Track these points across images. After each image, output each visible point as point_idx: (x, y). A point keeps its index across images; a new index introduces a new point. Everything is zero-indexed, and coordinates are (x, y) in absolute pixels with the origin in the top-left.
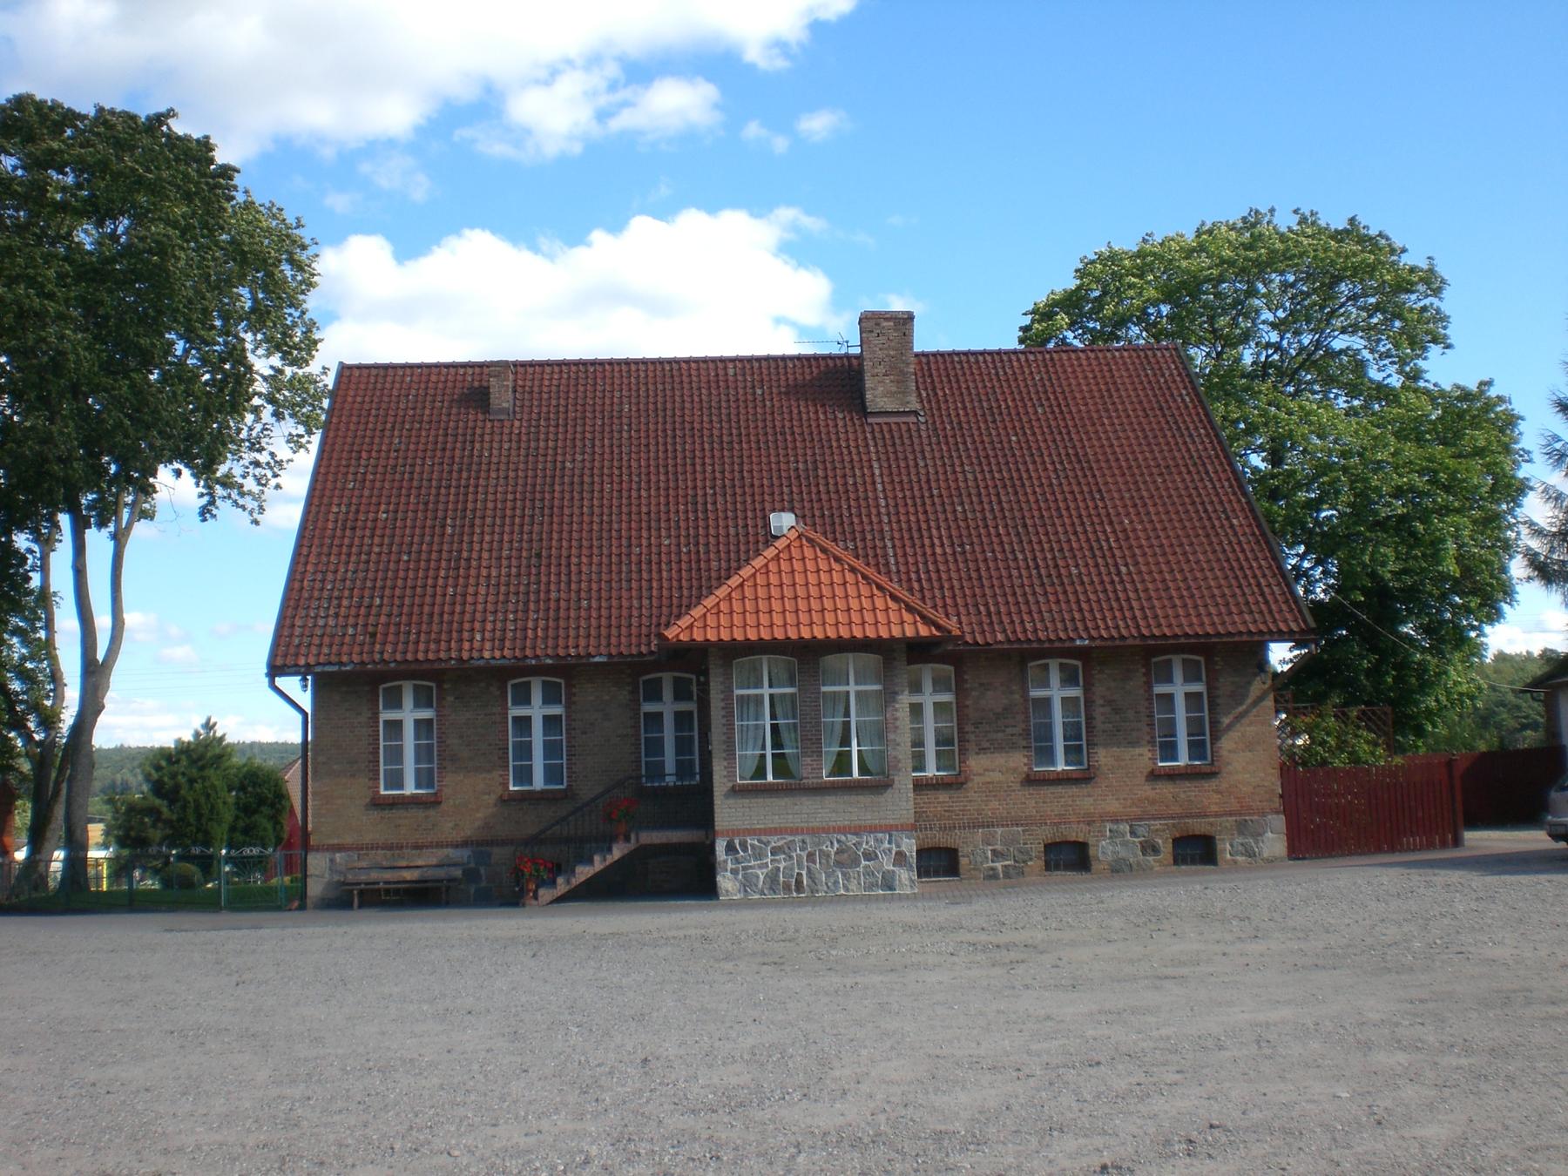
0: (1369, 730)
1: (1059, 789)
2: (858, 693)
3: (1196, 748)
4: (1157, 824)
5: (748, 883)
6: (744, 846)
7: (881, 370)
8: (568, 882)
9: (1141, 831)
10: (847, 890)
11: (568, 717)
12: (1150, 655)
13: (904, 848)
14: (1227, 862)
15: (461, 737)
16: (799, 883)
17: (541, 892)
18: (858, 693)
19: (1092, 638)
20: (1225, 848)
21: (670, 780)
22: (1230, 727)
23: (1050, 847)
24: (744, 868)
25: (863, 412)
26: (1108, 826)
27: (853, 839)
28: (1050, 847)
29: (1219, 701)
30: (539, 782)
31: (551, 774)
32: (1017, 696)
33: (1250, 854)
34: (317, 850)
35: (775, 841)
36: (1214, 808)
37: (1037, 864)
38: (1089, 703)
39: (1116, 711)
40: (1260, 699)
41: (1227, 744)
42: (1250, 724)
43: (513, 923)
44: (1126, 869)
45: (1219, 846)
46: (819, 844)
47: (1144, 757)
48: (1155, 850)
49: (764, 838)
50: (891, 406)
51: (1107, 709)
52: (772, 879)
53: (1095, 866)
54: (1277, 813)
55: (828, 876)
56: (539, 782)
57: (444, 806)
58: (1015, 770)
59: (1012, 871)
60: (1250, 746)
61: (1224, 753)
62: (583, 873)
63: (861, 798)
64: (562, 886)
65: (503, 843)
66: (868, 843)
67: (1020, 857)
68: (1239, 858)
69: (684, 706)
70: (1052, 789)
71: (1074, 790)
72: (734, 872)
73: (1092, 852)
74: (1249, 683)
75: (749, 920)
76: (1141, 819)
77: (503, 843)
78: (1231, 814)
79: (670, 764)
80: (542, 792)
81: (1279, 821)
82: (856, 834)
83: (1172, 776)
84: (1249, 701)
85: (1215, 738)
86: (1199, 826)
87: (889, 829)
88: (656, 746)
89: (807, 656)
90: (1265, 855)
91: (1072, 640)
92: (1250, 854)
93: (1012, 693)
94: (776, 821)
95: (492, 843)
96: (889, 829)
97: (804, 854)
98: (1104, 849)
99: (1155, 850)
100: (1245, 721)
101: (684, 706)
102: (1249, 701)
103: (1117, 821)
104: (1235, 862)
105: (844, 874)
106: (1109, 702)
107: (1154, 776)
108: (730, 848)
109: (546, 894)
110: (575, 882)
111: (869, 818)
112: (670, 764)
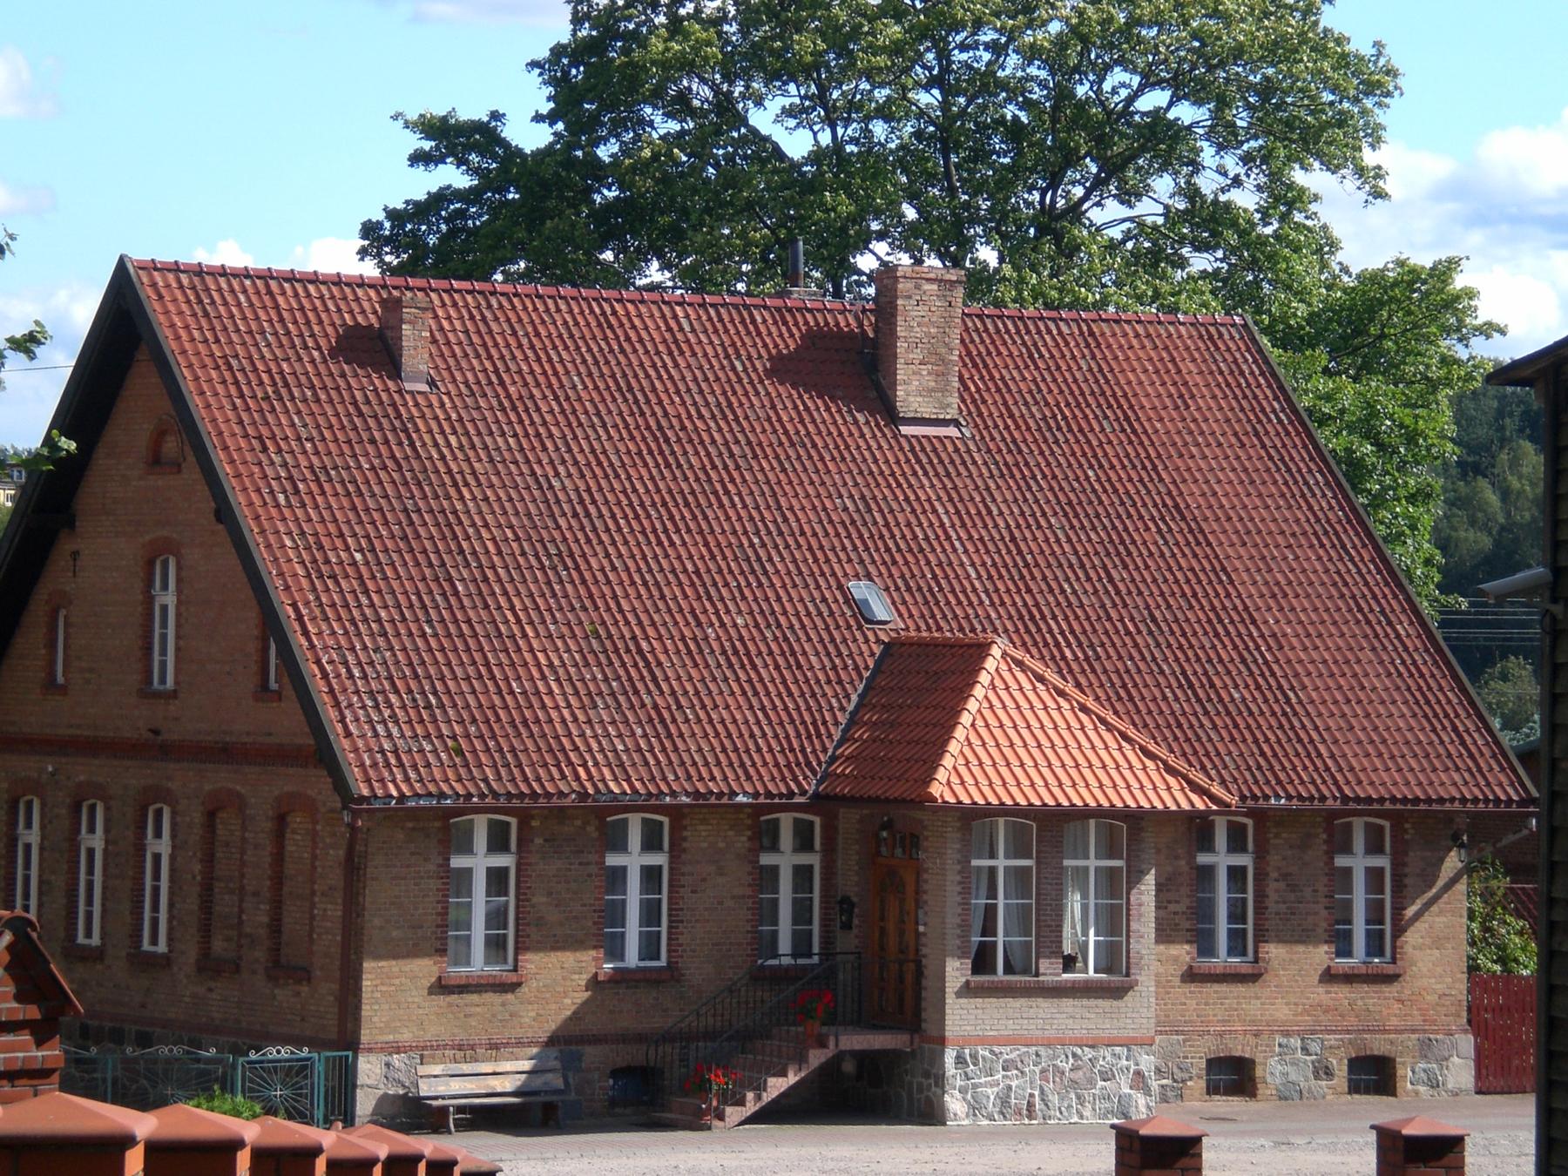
0: (1520, 916)
1: (1223, 988)
2: (1086, 869)
3: (1375, 944)
4: (1332, 1039)
5: (975, 1108)
6: (974, 1057)
7: (917, 355)
8: (759, 1098)
9: (1315, 1047)
10: (1082, 1117)
11: (671, 869)
12: (1328, 826)
13: (1142, 1067)
14: (1407, 1093)
15: (550, 894)
16: (1030, 1105)
17: (729, 1110)
18: (1086, 869)
19: (1289, 797)
20: (1406, 1073)
21: (786, 961)
22: (1418, 915)
23: (1214, 1064)
24: (975, 1086)
25: (893, 417)
26: (1279, 1039)
27: (1089, 1053)
28: (1214, 1064)
29: (1407, 881)
30: (632, 958)
31: (649, 947)
32: (1183, 863)
33: (1434, 1084)
34: (370, 1050)
35: (1009, 1054)
36: (1394, 1021)
37: (1198, 1085)
38: (1260, 876)
39: (1293, 888)
40: (1453, 881)
41: (1412, 938)
42: (1441, 912)
43: (924, 1153)
44: (1296, 1096)
45: (1400, 1072)
46: (1055, 1057)
47: (1321, 955)
48: (1329, 1073)
49: (996, 1049)
50: (927, 411)
51: (1282, 885)
52: (1004, 1101)
53: (1262, 1090)
54: (1465, 1031)
55: (1062, 1099)
56: (632, 958)
57: (524, 989)
58: (1176, 959)
59: (1170, 1094)
60: (1438, 942)
61: (1408, 949)
62: (777, 1086)
63: (1100, 1002)
64: (751, 1107)
65: (596, 1040)
66: (1105, 1057)
67: (1179, 1075)
68: (1422, 1089)
69: (804, 859)
70: (1216, 987)
71: (1240, 989)
72: (963, 1091)
73: (1259, 1072)
74: (1442, 860)
75: (979, 1158)
76: (1313, 1032)
77: (596, 1040)
78: (1414, 1031)
79: (785, 945)
80: (639, 970)
81: (1467, 1043)
82: (1092, 1047)
83: (1349, 978)
84: (1440, 883)
85: (1399, 930)
86: (1378, 1045)
87: (1127, 1044)
88: (770, 912)
89: (1050, 827)
90: (1450, 1086)
91: (1267, 798)
92: (1434, 1084)
93: (1177, 858)
94: (1009, 1028)
95: (583, 1040)
96: (1127, 1044)
97: (1037, 1070)
98: (1272, 1071)
99: (1329, 1073)
100: (1434, 908)
101: (804, 859)
102: (1440, 883)
103: (1287, 1034)
104: (1417, 1093)
105: (1078, 1097)
106: (1285, 876)
107: (1329, 977)
108: (960, 1060)
109: (734, 1114)
110: (767, 1097)
111: (1108, 1028)
112: (785, 945)
